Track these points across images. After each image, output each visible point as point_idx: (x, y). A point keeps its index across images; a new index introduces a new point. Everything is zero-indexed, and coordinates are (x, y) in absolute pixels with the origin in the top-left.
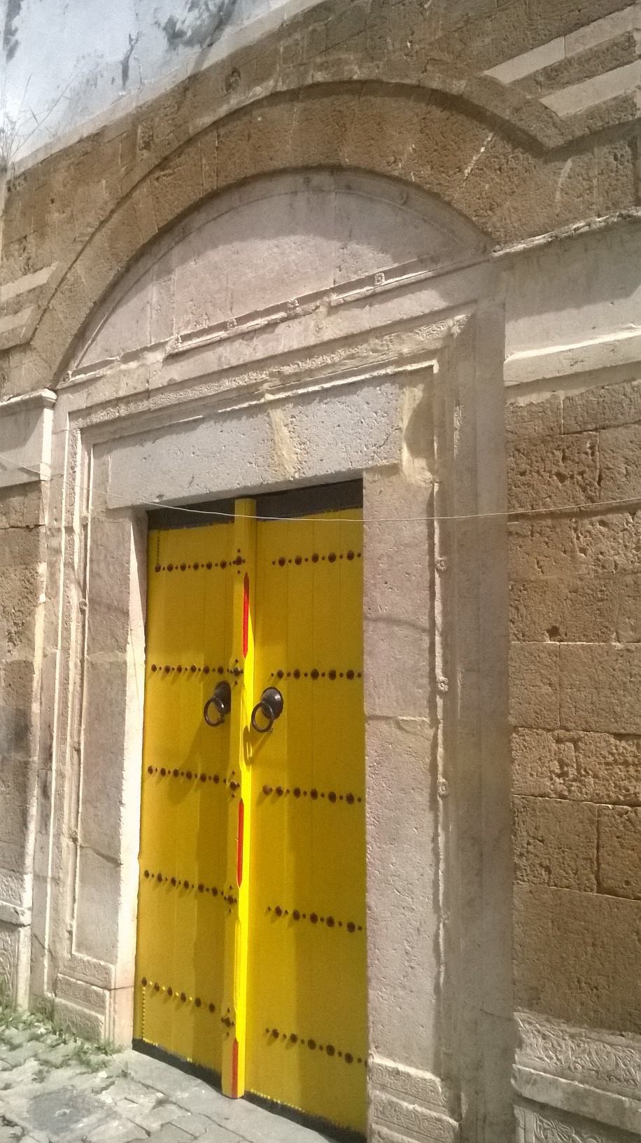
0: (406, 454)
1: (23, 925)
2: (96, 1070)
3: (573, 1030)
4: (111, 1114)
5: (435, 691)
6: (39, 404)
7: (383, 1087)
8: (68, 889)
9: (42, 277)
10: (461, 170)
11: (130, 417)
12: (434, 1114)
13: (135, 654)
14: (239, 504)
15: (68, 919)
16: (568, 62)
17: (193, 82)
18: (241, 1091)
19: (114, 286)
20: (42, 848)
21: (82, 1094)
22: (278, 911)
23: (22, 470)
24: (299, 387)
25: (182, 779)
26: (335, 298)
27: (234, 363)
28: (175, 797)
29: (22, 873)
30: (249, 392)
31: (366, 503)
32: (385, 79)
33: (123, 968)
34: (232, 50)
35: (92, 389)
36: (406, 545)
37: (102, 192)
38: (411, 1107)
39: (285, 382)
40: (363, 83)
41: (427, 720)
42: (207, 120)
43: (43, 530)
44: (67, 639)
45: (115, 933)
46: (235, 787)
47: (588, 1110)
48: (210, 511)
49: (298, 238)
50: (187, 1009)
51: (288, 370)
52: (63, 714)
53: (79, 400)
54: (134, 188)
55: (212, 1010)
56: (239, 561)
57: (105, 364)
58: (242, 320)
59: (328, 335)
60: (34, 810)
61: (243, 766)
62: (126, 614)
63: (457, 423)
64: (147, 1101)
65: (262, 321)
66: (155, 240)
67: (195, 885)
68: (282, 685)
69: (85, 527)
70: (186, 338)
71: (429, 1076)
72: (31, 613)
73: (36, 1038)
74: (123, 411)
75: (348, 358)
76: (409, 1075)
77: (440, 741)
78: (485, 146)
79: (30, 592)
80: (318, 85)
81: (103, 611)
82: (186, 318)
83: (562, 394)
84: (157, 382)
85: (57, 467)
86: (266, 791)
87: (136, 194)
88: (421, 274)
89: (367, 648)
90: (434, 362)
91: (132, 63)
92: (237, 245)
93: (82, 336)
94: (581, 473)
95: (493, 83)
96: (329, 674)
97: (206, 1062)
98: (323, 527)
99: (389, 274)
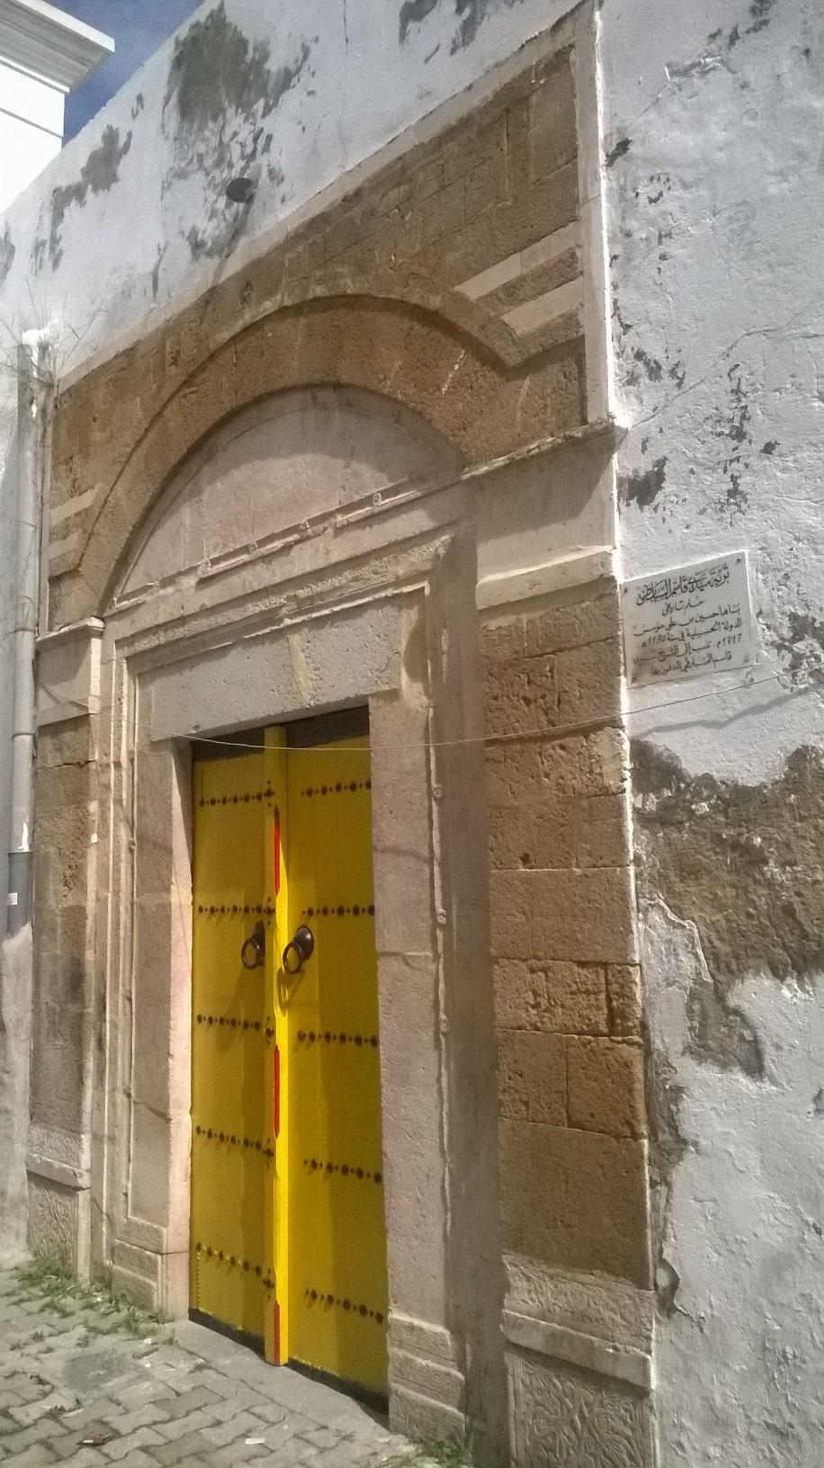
0: (404, 677)
1: (80, 1189)
2: (144, 1337)
3: (551, 1271)
4: (144, 1375)
5: (436, 925)
6: (85, 634)
7: (401, 1344)
8: (124, 1148)
9: (86, 500)
10: (439, 389)
11: (169, 644)
12: (444, 1369)
13: (181, 895)
14: (271, 735)
15: (123, 1181)
16: (522, 279)
17: (212, 296)
18: (284, 1358)
19: (150, 508)
20: (99, 1106)
21: (121, 1358)
22: (314, 1165)
23: (73, 703)
24: (313, 611)
25: (227, 1027)
26: (340, 519)
27: (257, 588)
28: (223, 1046)
29: (80, 1133)
30: (270, 617)
31: (372, 730)
32: (373, 293)
33: (176, 1232)
34: (247, 261)
35: (135, 616)
36: (408, 773)
37: (136, 410)
38: (424, 1363)
39: (303, 606)
40: (357, 297)
41: (430, 954)
42: (225, 335)
43: (93, 766)
44: (117, 881)
45: (167, 1195)
46: (271, 1033)
47: (565, 1352)
48: (238, 742)
49: (309, 457)
50: (237, 1273)
51: (302, 593)
52: (116, 962)
53: (122, 628)
54: (165, 406)
55: (258, 1273)
56: (269, 793)
57: (145, 589)
58: (262, 543)
59: (336, 557)
60: (90, 1065)
61: (278, 1012)
62: (170, 851)
63: (445, 647)
64: (185, 1366)
65: (278, 544)
66: (184, 461)
67: (238, 1138)
68: (313, 924)
69: (132, 761)
70: (214, 562)
71: (440, 1329)
72: (83, 856)
73: (91, 1306)
74: (162, 638)
75: (356, 579)
76: (421, 1330)
77: (441, 976)
78: (459, 362)
79: (82, 833)
80: (317, 300)
81: (150, 849)
82: (215, 540)
83: (524, 617)
84: (191, 608)
85: (105, 697)
86: (301, 1036)
87: (167, 412)
88: (411, 494)
89: (377, 882)
90: (425, 584)
91: (160, 272)
92: (258, 464)
93: (124, 561)
94: (544, 697)
95: (461, 299)
96: (345, 910)
97: (366, 1379)
98: (327, 756)
99: (386, 494)
